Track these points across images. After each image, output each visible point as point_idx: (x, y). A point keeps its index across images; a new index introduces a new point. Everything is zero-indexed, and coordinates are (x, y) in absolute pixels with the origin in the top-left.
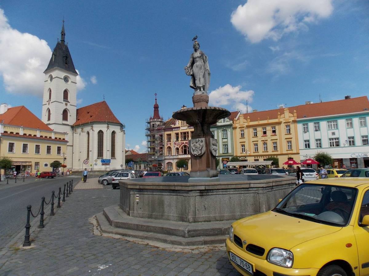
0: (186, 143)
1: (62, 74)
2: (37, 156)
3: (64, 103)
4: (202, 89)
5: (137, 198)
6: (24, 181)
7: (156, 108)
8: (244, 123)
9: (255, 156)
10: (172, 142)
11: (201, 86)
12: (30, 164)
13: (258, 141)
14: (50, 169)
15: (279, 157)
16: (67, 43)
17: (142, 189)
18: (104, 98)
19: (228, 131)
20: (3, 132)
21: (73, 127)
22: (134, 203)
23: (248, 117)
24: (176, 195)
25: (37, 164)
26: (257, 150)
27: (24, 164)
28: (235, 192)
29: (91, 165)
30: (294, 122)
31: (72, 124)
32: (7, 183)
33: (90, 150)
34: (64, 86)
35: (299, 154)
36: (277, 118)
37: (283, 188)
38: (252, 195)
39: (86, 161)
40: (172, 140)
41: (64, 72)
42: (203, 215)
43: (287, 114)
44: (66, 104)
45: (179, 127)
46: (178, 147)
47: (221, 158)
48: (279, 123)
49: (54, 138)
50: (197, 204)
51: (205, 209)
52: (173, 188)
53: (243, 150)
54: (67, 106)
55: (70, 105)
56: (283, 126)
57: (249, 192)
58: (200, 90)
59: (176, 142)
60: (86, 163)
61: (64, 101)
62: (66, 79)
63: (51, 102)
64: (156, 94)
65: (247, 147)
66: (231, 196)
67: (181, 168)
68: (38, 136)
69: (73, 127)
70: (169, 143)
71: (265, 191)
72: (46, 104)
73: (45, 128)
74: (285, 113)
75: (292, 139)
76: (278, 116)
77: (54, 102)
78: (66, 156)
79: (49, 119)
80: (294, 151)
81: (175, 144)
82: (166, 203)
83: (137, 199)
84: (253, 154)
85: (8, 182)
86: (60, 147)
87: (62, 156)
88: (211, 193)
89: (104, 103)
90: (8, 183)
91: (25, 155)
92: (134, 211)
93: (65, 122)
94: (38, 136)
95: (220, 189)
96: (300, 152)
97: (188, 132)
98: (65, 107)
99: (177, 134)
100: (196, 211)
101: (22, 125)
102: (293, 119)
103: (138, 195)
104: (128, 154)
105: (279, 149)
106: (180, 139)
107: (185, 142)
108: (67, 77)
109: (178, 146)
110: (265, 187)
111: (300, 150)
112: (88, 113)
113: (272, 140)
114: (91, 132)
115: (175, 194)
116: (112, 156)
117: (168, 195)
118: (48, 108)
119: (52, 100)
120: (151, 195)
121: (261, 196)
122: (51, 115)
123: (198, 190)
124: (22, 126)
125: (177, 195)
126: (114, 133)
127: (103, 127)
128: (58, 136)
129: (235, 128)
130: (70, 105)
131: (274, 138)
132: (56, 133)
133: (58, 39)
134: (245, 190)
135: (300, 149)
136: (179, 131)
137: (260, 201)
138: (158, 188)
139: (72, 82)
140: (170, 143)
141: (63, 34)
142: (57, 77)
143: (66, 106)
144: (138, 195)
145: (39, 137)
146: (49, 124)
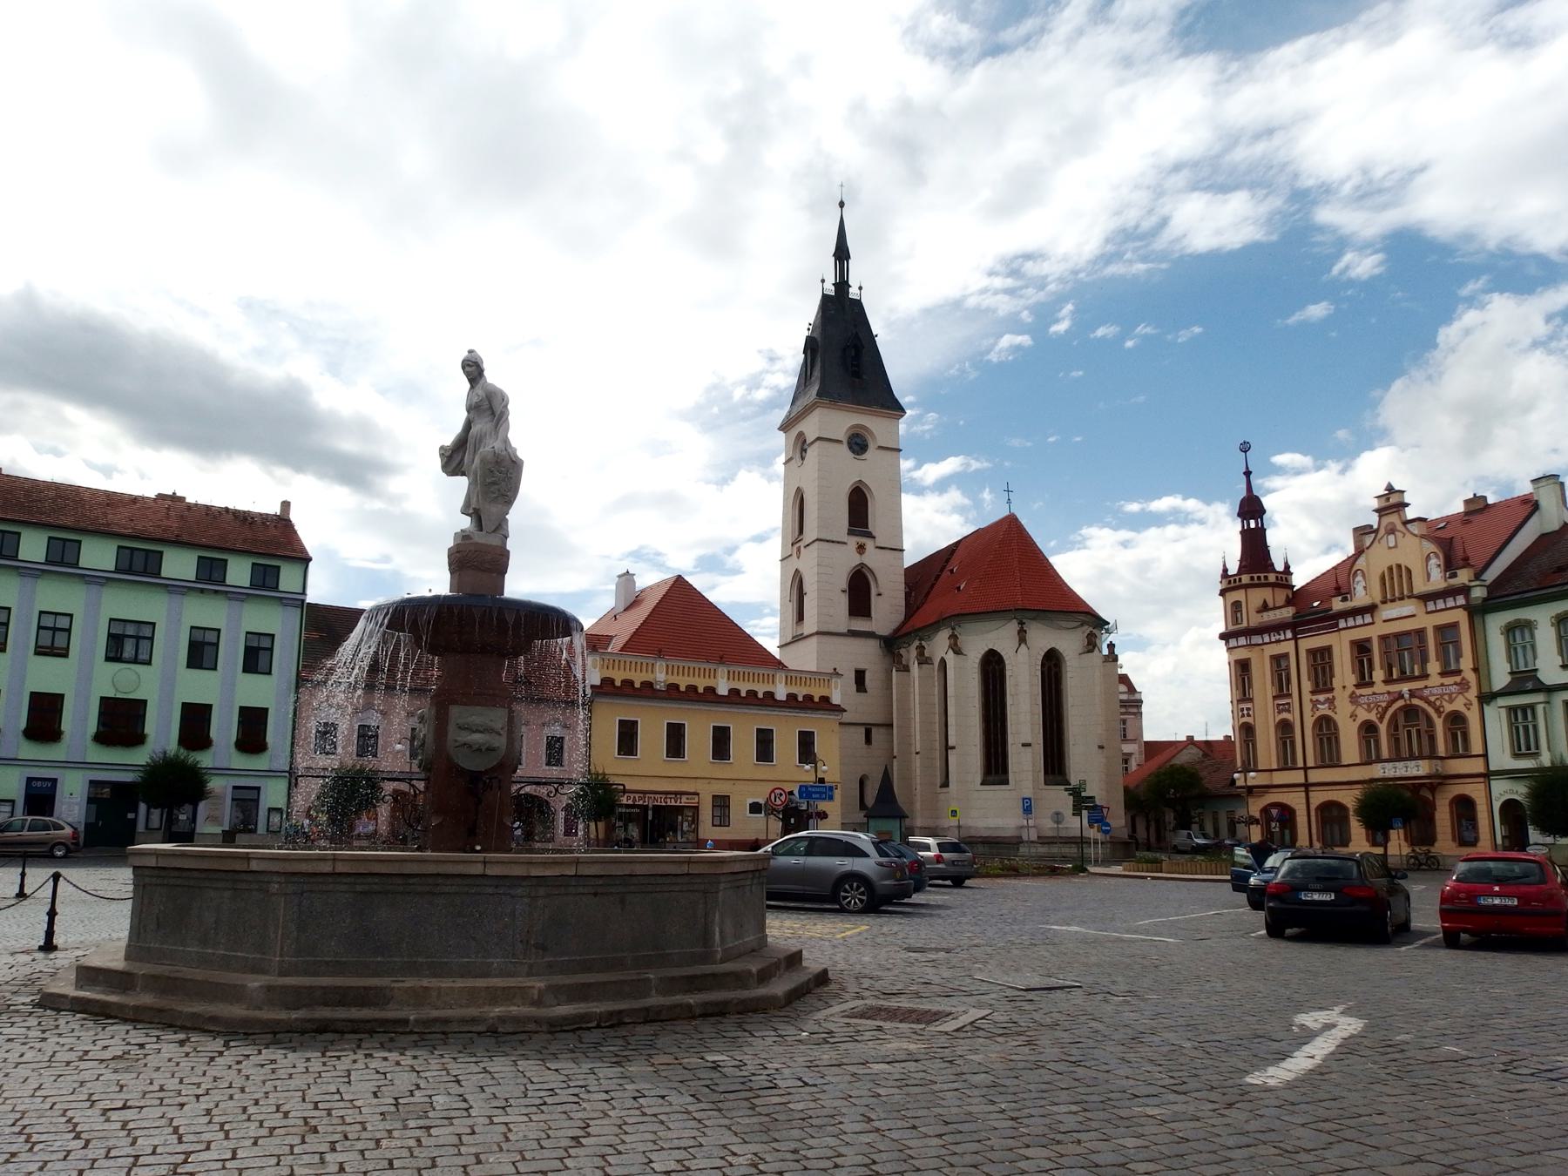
0: (1412, 694)
1: (840, 421)
2: (720, 770)
3: (853, 541)
10: (1337, 692)
20: (598, 682)
21: (892, 644)
25: (722, 804)
29: (954, 813)
34: (850, 470)
40: (1336, 683)
44: (861, 548)
45: (1371, 609)
46: (1373, 717)
59: (1359, 692)
61: (850, 533)
62: (858, 443)
64: (1245, 448)
68: (723, 690)
69: (892, 644)
70: (1321, 698)
81: (1354, 699)
90: (58, 940)
91: (675, 767)
93: (860, 625)
97: (1421, 633)
98: (855, 560)
99: (1361, 648)
106: (1379, 675)
107: (1405, 688)
108: (862, 432)
109: (1369, 710)
119: (811, 533)
126: (1052, 664)
127: (1000, 637)
128: (801, 692)
132: (794, 676)
136: (1373, 632)
141: (842, 253)
142: (819, 439)
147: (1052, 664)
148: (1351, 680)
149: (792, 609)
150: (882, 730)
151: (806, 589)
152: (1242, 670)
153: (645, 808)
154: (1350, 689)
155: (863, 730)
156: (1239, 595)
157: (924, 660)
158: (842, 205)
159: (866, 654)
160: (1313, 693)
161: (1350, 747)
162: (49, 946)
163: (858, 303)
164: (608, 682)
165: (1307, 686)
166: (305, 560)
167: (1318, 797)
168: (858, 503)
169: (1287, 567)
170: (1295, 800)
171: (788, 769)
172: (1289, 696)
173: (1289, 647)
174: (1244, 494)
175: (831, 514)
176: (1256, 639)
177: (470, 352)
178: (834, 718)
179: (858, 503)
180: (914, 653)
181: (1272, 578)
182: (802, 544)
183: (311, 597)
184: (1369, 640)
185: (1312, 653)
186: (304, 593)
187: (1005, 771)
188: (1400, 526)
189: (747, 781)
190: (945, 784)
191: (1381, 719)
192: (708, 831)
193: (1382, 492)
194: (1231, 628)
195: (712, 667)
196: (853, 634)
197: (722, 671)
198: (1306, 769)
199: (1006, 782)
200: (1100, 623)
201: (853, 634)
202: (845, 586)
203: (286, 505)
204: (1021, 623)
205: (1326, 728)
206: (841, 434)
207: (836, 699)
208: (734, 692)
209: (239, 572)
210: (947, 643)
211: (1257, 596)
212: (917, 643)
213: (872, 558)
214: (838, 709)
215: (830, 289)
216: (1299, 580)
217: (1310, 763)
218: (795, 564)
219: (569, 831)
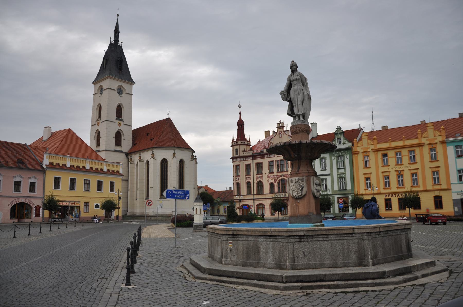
1: (115, 84)
2: (87, 194)
3: (117, 122)
4: (302, 118)
5: (230, 244)
6: (67, 228)
7: (241, 124)
8: (369, 146)
9: (385, 194)
10: (264, 175)
11: (300, 113)
13: (389, 172)
14: (102, 213)
15: (421, 195)
16: (122, 43)
17: (236, 235)
18: (168, 114)
19: (346, 158)
20: (48, 164)
21: (127, 154)
22: (227, 250)
23: (375, 137)
24: (272, 241)
25: (86, 204)
26: (388, 185)
28: (337, 239)
30: (442, 142)
31: (126, 150)
33: (150, 186)
34: (117, 99)
35: (450, 189)
36: (416, 138)
37: (394, 234)
38: (356, 241)
40: (264, 172)
41: (119, 81)
42: (303, 261)
43: (431, 132)
44: (120, 124)
46: (273, 181)
47: (336, 198)
48: (421, 145)
50: (295, 251)
51: (305, 256)
52: (269, 234)
53: (368, 185)
56: (426, 150)
57: (353, 238)
58: (299, 119)
59: (270, 175)
60: (149, 205)
61: (117, 119)
62: (120, 91)
63: (102, 120)
64: (240, 106)
65: (373, 181)
66: (333, 242)
67: (277, 212)
68: (68, 165)
69: (127, 154)
71: (371, 237)
73: (92, 154)
74: (428, 130)
75: (440, 169)
76: (418, 135)
79: (98, 144)
80: (444, 186)
81: (268, 177)
82: (262, 250)
83: (230, 246)
84: (382, 191)
88: (311, 239)
90: (30, 233)
91: (72, 193)
92: (227, 258)
93: (118, 148)
94: (68, 165)
95: (320, 235)
96: (452, 187)
98: (118, 128)
100: (295, 258)
101: (68, 154)
102: (440, 139)
103: (231, 242)
104: (200, 191)
105: (420, 182)
110: (371, 233)
111: (452, 185)
112: (148, 134)
113: (410, 170)
114: (151, 161)
115: (272, 240)
117: (264, 241)
119: (103, 117)
120: (245, 242)
121: (366, 242)
122: (101, 139)
123: (296, 236)
125: (274, 241)
126: (181, 163)
127: (166, 154)
128: (111, 169)
129: (357, 153)
131: (413, 167)
132: (109, 164)
133: (111, 38)
134: (348, 235)
135: (451, 182)
137: (365, 247)
138: (253, 233)
139: (127, 93)
140: (261, 175)
141: (117, 31)
142: (108, 88)
143: (119, 126)
144: (231, 242)
146: (99, 151)
147: (181, 163)
148: (268, 171)
152: (237, 168)
154: (267, 174)
156: (237, 147)
158: (118, 15)
159: (121, 158)
160: (257, 174)
161: (266, 189)
163: (121, 47)
164: (51, 163)
165: (255, 173)
167: (257, 202)
168: (119, 110)
169: (249, 140)
170: (250, 203)
171: (106, 194)
172: (250, 175)
173: (250, 162)
174: (239, 119)
175: (109, 112)
176: (242, 159)
177: (293, 61)
178: (121, 178)
179: (119, 110)
181: (246, 143)
182: (100, 121)
184: (273, 161)
185: (257, 164)
188: (283, 132)
189: (96, 198)
190: (136, 200)
191: (275, 182)
192: (83, 215)
193: (278, 123)
194: (235, 155)
195: (85, 160)
196: (116, 151)
197: (88, 161)
198: (254, 195)
200: (194, 152)
201: (116, 151)
204: (174, 151)
205: (260, 185)
207: (121, 172)
208: (91, 168)
210: (151, 155)
211: (242, 148)
214: (121, 175)
215: (113, 42)
216: (252, 144)
217: (255, 193)
218: (96, 127)
219: (38, 214)
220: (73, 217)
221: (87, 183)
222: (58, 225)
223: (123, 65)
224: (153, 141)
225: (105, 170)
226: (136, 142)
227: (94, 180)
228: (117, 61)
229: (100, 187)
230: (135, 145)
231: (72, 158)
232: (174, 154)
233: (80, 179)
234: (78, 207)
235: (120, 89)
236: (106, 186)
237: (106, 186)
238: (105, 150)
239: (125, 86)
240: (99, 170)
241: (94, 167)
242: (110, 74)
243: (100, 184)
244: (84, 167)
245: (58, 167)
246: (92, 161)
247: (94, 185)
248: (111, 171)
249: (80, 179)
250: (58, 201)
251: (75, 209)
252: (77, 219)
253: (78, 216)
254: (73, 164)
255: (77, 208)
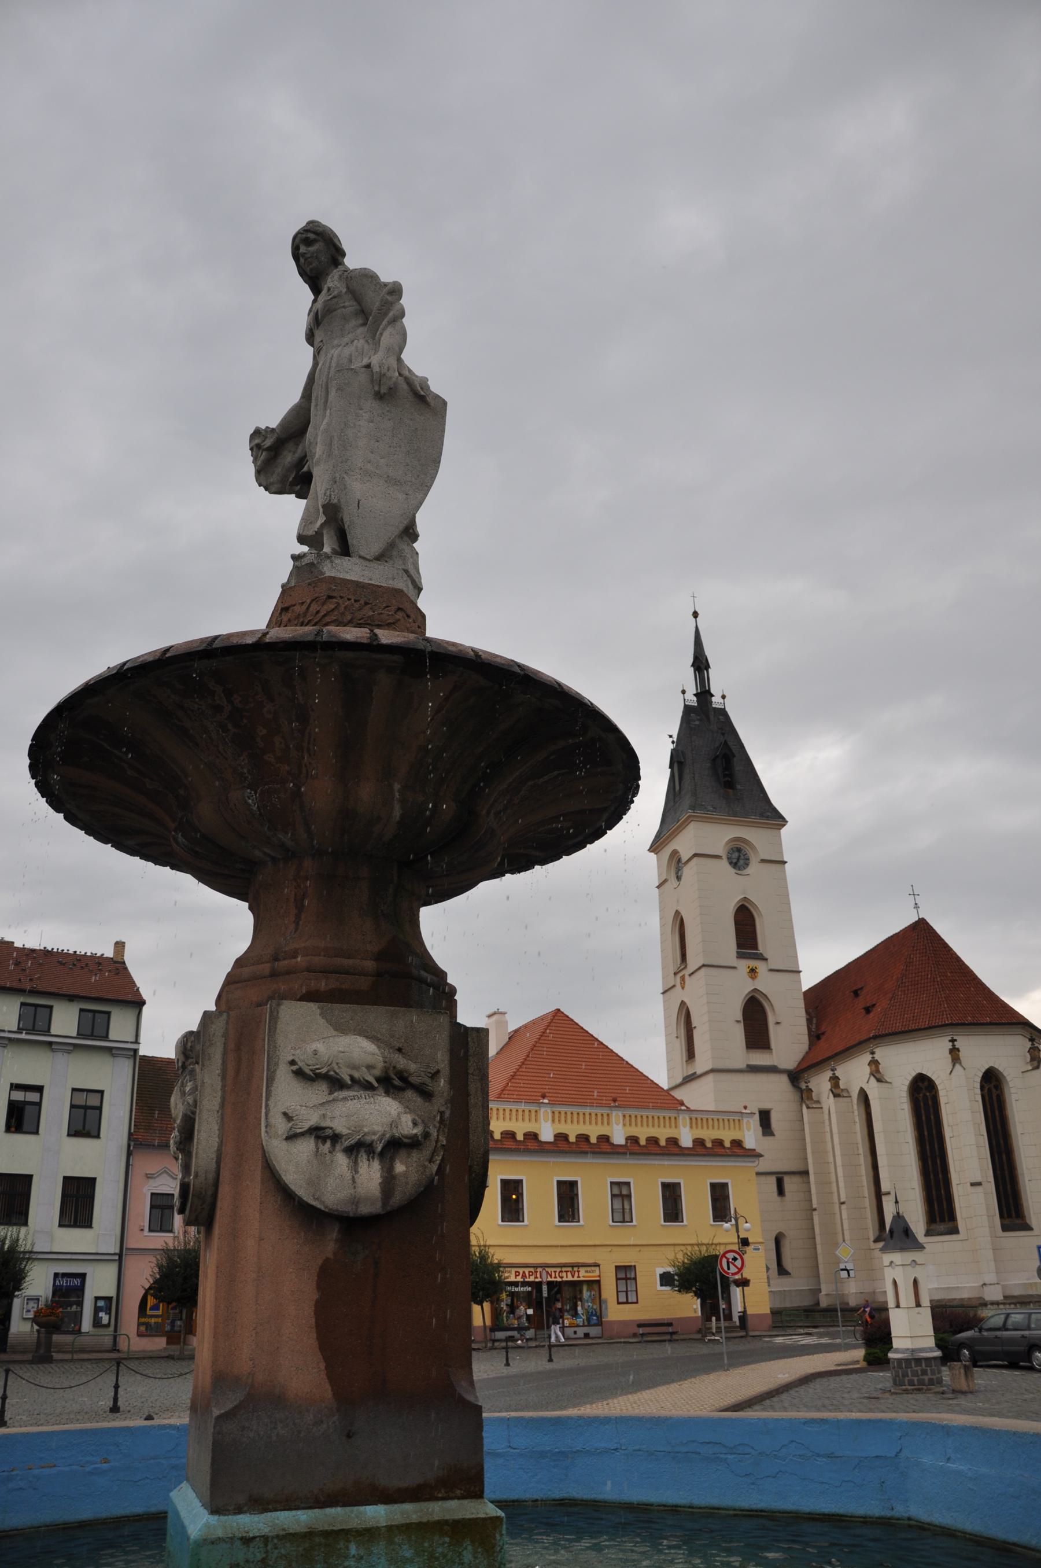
3: (744, 965)
12: (592, 1275)
16: (724, 697)
18: (916, 906)
21: (796, 1077)
25: (626, 1274)
27: (570, 1278)
31: (790, 1064)
32: (111, 1404)
34: (731, 888)
39: (735, 1259)
44: (753, 971)
49: (551, 1139)
54: (756, 980)
55: (771, 970)
61: (740, 956)
62: (738, 857)
63: (691, 968)
69: (796, 1077)
72: (674, 986)
77: (699, 968)
78: (747, 1230)
85: (116, 1399)
86: (573, 1184)
87: (727, 1231)
89: (921, 930)
93: (759, 1058)
94: (547, 1134)
98: (747, 986)
101: (544, 1097)
112: (856, 993)
114: (873, 1090)
116: (1010, 1216)
118: (683, 1003)
119: (693, 962)
124: (546, 1101)
126: (992, 1084)
128: (709, 1135)
130: (771, 970)
132: (698, 1117)
133: (684, 692)
139: (763, 861)
141: (700, 664)
142: (696, 855)
143: (753, 978)
145: (623, 1142)
147: (992, 1084)
149: (680, 1046)
150: (796, 1179)
151: (694, 1023)
153: (537, 1286)
155: (773, 1180)
157: (837, 1090)
158: (695, 615)
159: (775, 1093)
162: (115, 1409)
163: (723, 712)
166: (139, 1003)
168: (745, 923)
171: (699, 1231)
179: (745, 923)
180: (827, 1085)
182: (686, 972)
183: (144, 1051)
186: (137, 1042)
187: (952, 1216)
189: (656, 1247)
192: (615, 1313)
195: (605, 1111)
197: (617, 1115)
199: (955, 1231)
202: (739, 1016)
203: (120, 946)
204: (953, 1041)
206: (720, 849)
207: (750, 1143)
208: (633, 1140)
209: (65, 1021)
212: (829, 1074)
213: (766, 983)
214: (754, 1155)
215: (692, 700)
220: (580, 1321)
221: (621, 1193)
222: (504, 1352)
223: (738, 767)
224: (871, 1015)
225: (686, 1142)
226: (823, 1029)
227: (646, 1183)
228: (714, 760)
229: (673, 1211)
230: (818, 1037)
231: (557, 1109)
232: (954, 1052)
233: (594, 1183)
234: (595, 1284)
235: (739, 850)
236: (696, 1203)
237: (696, 1203)
238: (712, 1071)
239: (754, 836)
240: (663, 1143)
241: (643, 1133)
242: (693, 808)
243: (671, 1195)
244: (673, 1142)
245: (509, 1144)
246: (633, 1112)
247: (647, 1202)
248: (709, 1145)
249: (594, 1183)
250: (499, 1265)
251: (586, 1294)
252: (594, 1331)
253: (596, 1318)
254: (563, 1128)
255: (589, 1290)
